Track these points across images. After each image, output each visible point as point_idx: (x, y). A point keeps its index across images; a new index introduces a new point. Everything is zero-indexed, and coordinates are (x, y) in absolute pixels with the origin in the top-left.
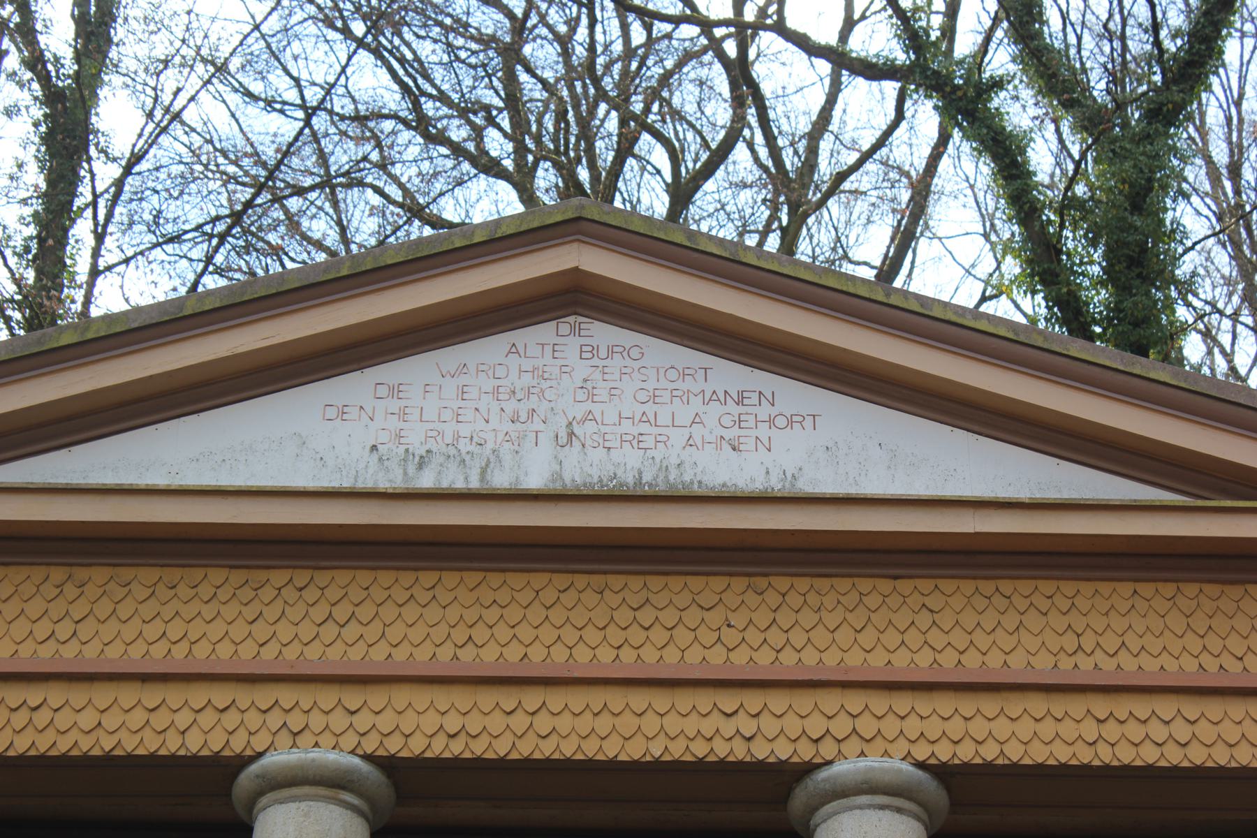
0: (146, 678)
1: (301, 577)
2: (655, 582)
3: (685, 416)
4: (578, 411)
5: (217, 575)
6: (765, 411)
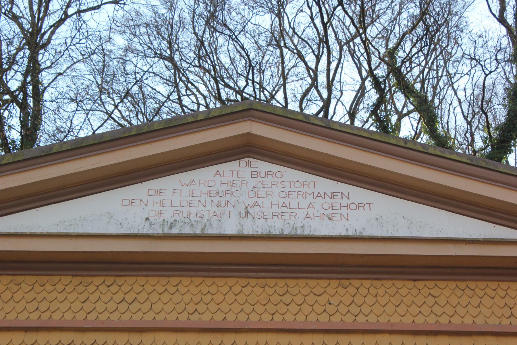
0: (27, 330)
1: (109, 280)
2: (292, 283)
3: (304, 204)
4: (251, 202)
5: (66, 280)
6: (345, 201)
